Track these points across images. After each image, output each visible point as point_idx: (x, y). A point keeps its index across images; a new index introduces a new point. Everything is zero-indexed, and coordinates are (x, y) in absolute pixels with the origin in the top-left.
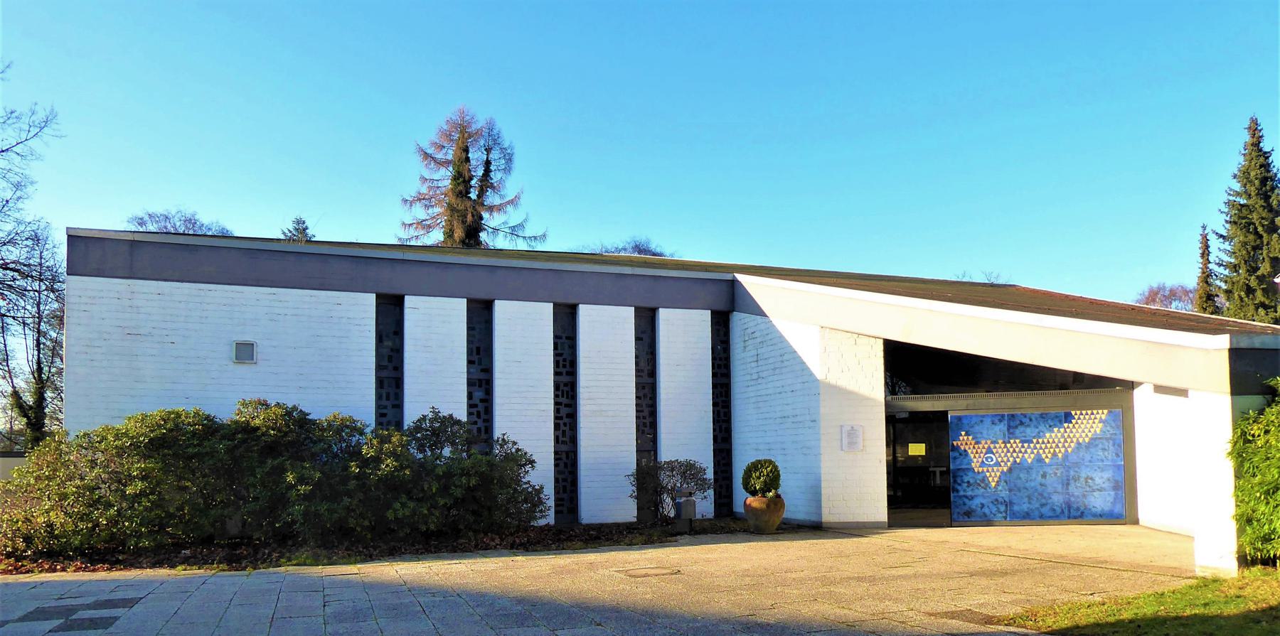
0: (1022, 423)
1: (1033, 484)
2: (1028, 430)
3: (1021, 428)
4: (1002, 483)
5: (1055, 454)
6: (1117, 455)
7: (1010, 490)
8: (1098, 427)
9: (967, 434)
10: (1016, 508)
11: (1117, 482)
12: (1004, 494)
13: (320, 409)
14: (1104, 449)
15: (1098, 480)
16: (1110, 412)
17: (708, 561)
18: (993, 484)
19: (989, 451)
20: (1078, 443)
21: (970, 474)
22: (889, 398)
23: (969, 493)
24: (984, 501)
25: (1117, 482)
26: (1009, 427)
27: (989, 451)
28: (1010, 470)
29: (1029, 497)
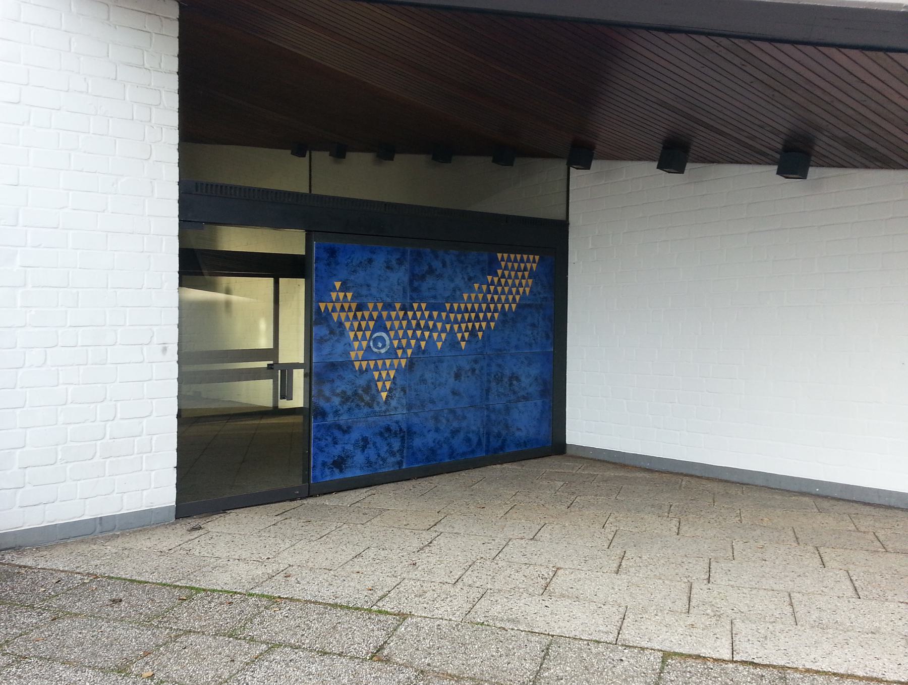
0: (431, 271)
3: (430, 281)
4: (398, 393)
6: (548, 337)
7: (410, 407)
8: (527, 286)
9: (344, 288)
14: (533, 325)
18: (384, 395)
26: (413, 277)
27: (380, 325)
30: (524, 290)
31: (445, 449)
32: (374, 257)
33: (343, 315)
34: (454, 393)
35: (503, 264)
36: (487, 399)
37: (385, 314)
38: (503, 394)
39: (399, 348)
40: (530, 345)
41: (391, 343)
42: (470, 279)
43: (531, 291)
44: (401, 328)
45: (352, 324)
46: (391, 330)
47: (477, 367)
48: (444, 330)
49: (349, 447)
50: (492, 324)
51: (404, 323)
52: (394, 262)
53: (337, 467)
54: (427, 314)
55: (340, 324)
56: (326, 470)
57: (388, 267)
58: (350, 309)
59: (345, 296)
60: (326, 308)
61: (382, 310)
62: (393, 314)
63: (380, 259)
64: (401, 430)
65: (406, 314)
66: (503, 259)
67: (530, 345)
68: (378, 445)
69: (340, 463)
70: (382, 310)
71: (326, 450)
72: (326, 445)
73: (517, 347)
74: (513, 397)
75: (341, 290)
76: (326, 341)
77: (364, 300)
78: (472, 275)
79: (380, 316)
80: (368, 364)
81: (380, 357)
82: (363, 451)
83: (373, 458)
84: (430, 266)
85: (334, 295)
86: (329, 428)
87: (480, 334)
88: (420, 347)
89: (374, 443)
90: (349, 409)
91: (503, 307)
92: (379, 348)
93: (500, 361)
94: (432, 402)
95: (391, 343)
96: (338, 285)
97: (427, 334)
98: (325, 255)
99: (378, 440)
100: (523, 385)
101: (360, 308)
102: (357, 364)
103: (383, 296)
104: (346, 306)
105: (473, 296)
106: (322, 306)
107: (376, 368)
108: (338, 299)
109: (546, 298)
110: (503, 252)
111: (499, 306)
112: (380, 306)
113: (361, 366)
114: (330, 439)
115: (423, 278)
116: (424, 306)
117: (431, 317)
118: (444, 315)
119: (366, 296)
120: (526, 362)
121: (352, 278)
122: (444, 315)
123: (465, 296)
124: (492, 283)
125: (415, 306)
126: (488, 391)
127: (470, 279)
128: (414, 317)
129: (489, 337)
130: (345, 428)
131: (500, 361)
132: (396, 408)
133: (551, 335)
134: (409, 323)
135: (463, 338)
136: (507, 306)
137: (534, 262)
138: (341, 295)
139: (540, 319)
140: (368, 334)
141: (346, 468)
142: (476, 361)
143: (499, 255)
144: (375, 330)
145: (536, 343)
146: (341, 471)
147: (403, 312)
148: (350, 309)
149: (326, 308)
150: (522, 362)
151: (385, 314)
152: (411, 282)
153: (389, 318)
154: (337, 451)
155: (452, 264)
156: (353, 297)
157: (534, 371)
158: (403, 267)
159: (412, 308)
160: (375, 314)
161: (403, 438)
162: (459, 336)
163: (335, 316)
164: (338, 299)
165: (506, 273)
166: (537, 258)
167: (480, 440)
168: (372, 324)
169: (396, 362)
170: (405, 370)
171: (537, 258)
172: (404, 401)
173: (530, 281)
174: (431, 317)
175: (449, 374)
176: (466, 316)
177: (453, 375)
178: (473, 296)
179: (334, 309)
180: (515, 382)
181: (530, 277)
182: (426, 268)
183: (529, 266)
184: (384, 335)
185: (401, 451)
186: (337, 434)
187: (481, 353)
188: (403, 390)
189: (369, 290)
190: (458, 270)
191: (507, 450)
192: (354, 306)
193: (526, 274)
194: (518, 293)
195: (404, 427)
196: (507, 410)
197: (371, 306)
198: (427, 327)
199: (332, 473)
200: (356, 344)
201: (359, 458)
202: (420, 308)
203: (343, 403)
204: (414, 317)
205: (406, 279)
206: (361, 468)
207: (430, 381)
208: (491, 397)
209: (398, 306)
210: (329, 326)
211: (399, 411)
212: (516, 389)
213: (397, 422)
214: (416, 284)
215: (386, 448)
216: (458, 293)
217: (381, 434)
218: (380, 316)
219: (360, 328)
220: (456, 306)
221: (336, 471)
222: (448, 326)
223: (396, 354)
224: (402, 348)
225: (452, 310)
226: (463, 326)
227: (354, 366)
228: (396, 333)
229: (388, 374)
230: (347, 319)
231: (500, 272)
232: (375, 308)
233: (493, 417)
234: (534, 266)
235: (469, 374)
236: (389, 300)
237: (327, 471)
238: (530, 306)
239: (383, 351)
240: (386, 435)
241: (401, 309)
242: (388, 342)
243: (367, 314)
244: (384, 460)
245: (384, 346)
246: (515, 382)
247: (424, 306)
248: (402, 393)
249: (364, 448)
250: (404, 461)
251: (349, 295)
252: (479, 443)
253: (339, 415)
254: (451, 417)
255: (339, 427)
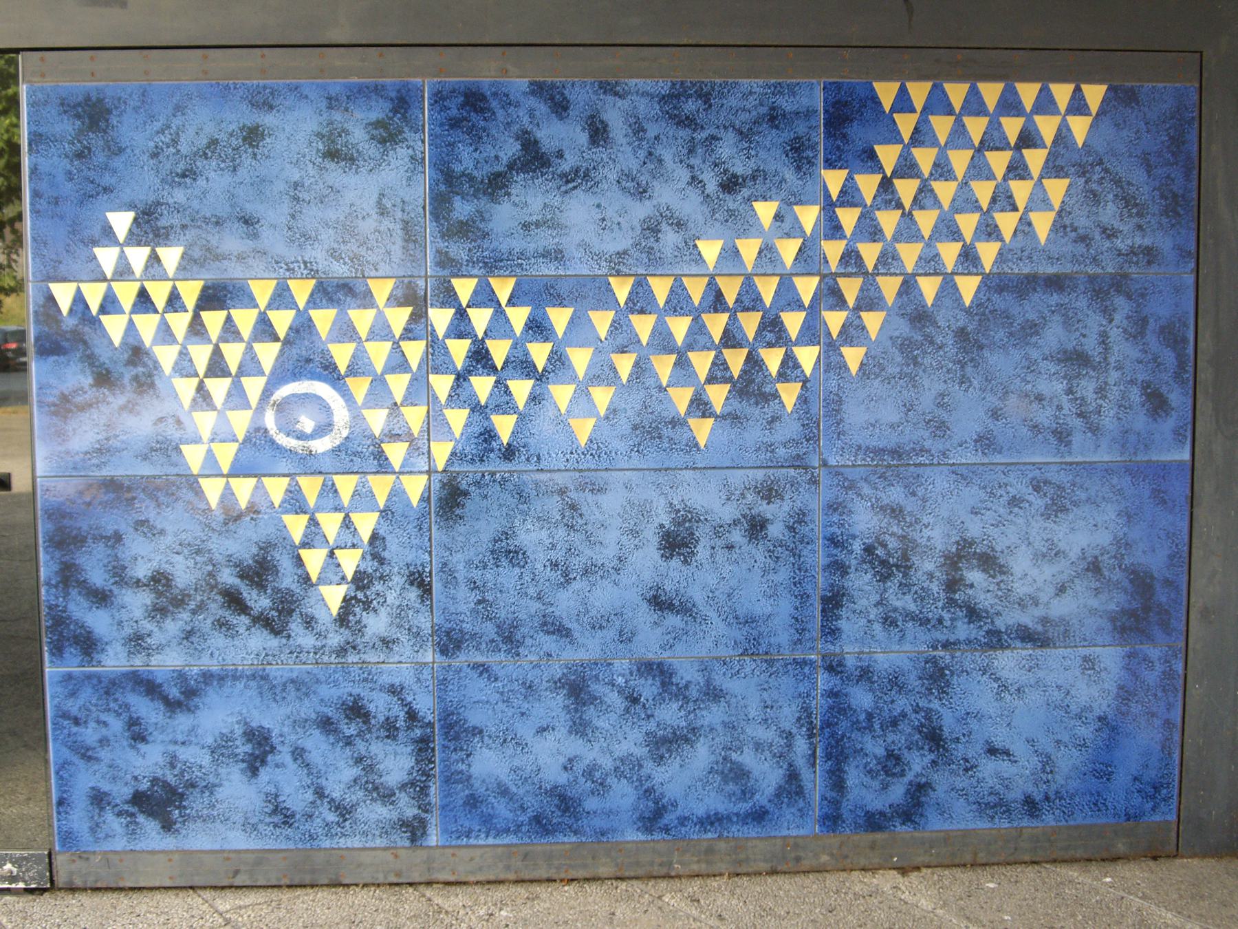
0: (534, 159)
1: (603, 596)
2: (578, 211)
3: (531, 197)
4: (395, 592)
5: (752, 386)
6: (1157, 403)
7: (450, 641)
8: (1041, 207)
9: (150, 228)
10: (487, 764)
11: (1141, 582)
12: (408, 666)
13: (743, 240)
14: (1076, 359)
15: (1028, 573)
16: (1119, 97)
17: (263, 73)
18: (334, 596)
19: (304, 358)
20: (920, 317)
21: (175, 522)
22: (486, 424)
23: (168, 661)
24: (271, 718)
25: (1141, 582)
26: (448, 184)
27: (304, 358)
28: (451, 498)
29: (577, 689)
30: (1025, 222)
31: (623, 795)
32: (268, 120)
33: (147, 325)
34: (659, 603)
35: (906, 124)
36: (831, 633)
37: (323, 319)
38: (910, 617)
39: (394, 437)
40: (1062, 436)
41: (357, 417)
42: (731, 184)
43: (1059, 227)
44: (399, 364)
45: (184, 354)
46: (353, 371)
47: (777, 513)
48: (603, 374)
49: (196, 757)
50: (853, 356)
51: (415, 351)
52: (358, 136)
53: (151, 814)
54: (518, 317)
55: (136, 352)
56: (109, 816)
57: (332, 155)
58: (174, 302)
59: (154, 259)
60: (79, 299)
61: (511, 302)
62: (362, 319)
63: (295, 129)
64: (412, 716)
65: (419, 316)
66: (903, 103)
67: (1062, 436)
68: (315, 757)
69: (160, 802)
70: (313, 302)
71: (104, 754)
72: (104, 742)
73: (985, 442)
74: (963, 630)
75: (134, 238)
76: (83, 408)
77: (234, 271)
78: (740, 168)
79: (303, 327)
80: (259, 488)
81: (306, 463)
82: (253, 771)
83: (297, 798)
84: (529, 144)
85: (107, 257)
86: (110, 687)
87: (789, 394)
88: (489, 435)
89: (298, 753)
90: (189, 635)
91: (908, 286)
92: (301, 436)
93: (895, 495)
94: (560, 631)
95: (357, 417)
96: (121, 221)
97: (521, 389)
98: (66, 127)
99: (317, 745)
100: (1021, 589)
101: (213, 298)
102: (212, 489)
103: (317, 254)
104: (159, 293)
105: (749, 249)
106: (63, 294)
107: (295, 503)
108: (123, 272)
109: (1150, 255)
110: (901, 74)
111: (889, 287)
112: (302, 290)
113: (228, 493)
114: (117, 725)
115: (496, 185)
116: (503, 289)
117: (538, 328)
118: (602, 321)
119: (241, 258)
120: (1039, 502)
121: (179, 196)
122: (602, 321)
123: (710, 250)
124: (849, 196)
125: (464, 288)
126: (833, 602)
127: (731, 184)
128: (461, 327)
129: (835, 405)
130: (174, 693)
131: (895, 495)
132: (387, 643)
133: (1177, 397)
134: (436, 348)
135: (700, 406)
136: (929, 287)
137: (1078, 106)
138: (138, 256)
139: (1115, 334)
140: (254, 386)
141: (186, 819)
142: (769, 493)
143: (886, 92)
144: (281, 375)
145: (1094, 430)
146: (168, 826)
147: (406, 312)
148: (174, 302)
149: (79, 299)
150: (1015, 502)
151: (323, 319)
152: (440, 203)
153: (346, 331)
154: (147, 763)
155: (638, 130)
156: (188, 266)
157: (1087, 532)
158: (402, 152)
159: (448, 297)
160: (282, 321)
161: (423, 746)
162: (681, 398)
163: (115, 326)
164: (123, 272)
165: (925, 158)
166: (1095, 94)
167: (793, 776)
168: (268, 353)
169: (381, 486)
170: (424, 515)
171: (1095, 94)
172: (424, 622)
173: (1057, 189)
174: (538, 328)
175: (635, 533)
176: (716, 324)
177: (652, 538)
178: (749, 249)
179: (110, 304)
180: (975, 576)
181: (1053, 168)
182: (510, 149)
183: (1047, 127)
184: (322, 389)
185: (417, 787)
186: (148, 710)
187: (798, 462)
188: (420, 581)
189: (255, 236)
190: (667, 155)
191: (935, 824)
192: (190, 292)
193: (1035, 159)
194: (989, 231)
195: (425, 705)
196: (937, 677)
197: (262, 291)
198: (525, 367)
199: (132, 831)
200: (205, 422)
201: (238, 791)
202: (485, 297)
203: (159, 612)
204: (461, 327)
205: (419, 191)
206: (249, 827)
207: (539, 558)
208: (849, 625)
209: (382, 290)
210: (90, 359)
211: (405, 650)
212: (985, 600)
213: (395, 691)
214: (462, 209)
215: (351, 773)
216: (670, 238)
217: (326, 724)
218: (303, 327)
219: (217, 367)
220: (661, 288)
221: (150, 826)
222: (625, 365)
223: (380, 456)
224: (409, 437)
225: (640, 301)
226: (702, 362)
227: (199, 493)
228: (379, 383)
229: (347, 524)
230: (165, 334)
231: (888, 155)
232: (282, 298)
233: (862, 698)
234: (1080, 127)
235: (737, 536)
236: (340, 270)
237: (114, 823)
238: (1055, 283)
239: (322, 445)
240: (350, 730)
241: (396, 300)
242: (341, 415)
243: (245, 319)
244: (344, 811)
245: (324, 429)
246: (975, 576)
247: (503, 289)
248: (413, 594)
249: (254, 765)
250: (434, 820)
251: (171, 256)
252: (792, 786)
253: (149, 651)
254: (648, 689)
255: (149, 687)
